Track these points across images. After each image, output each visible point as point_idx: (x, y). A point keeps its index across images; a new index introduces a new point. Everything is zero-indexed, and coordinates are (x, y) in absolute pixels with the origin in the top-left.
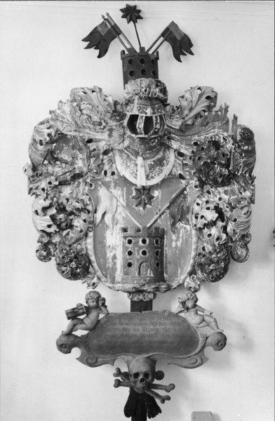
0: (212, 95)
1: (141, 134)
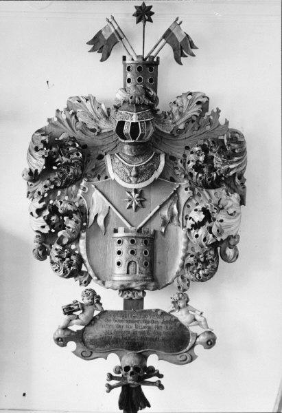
0: (204, 100)
1: (129, 139)
